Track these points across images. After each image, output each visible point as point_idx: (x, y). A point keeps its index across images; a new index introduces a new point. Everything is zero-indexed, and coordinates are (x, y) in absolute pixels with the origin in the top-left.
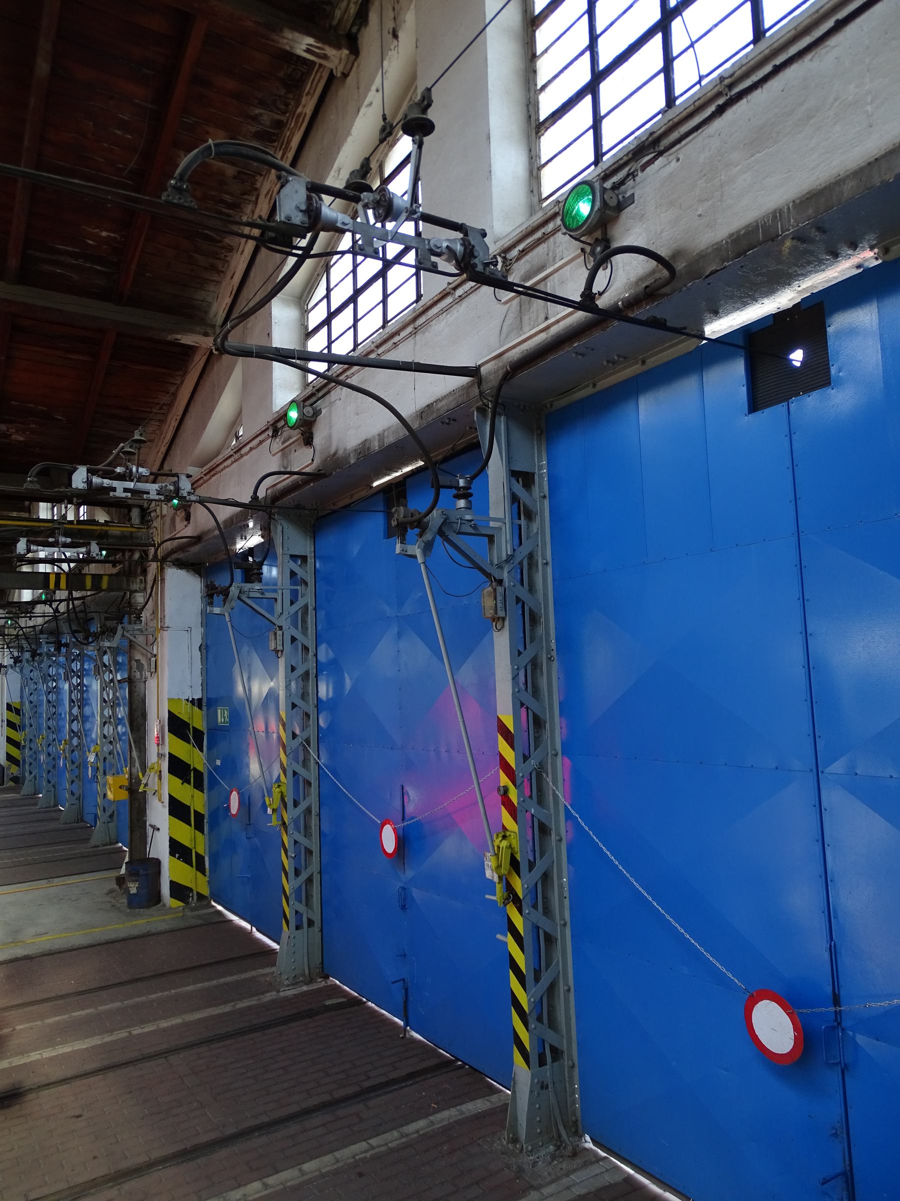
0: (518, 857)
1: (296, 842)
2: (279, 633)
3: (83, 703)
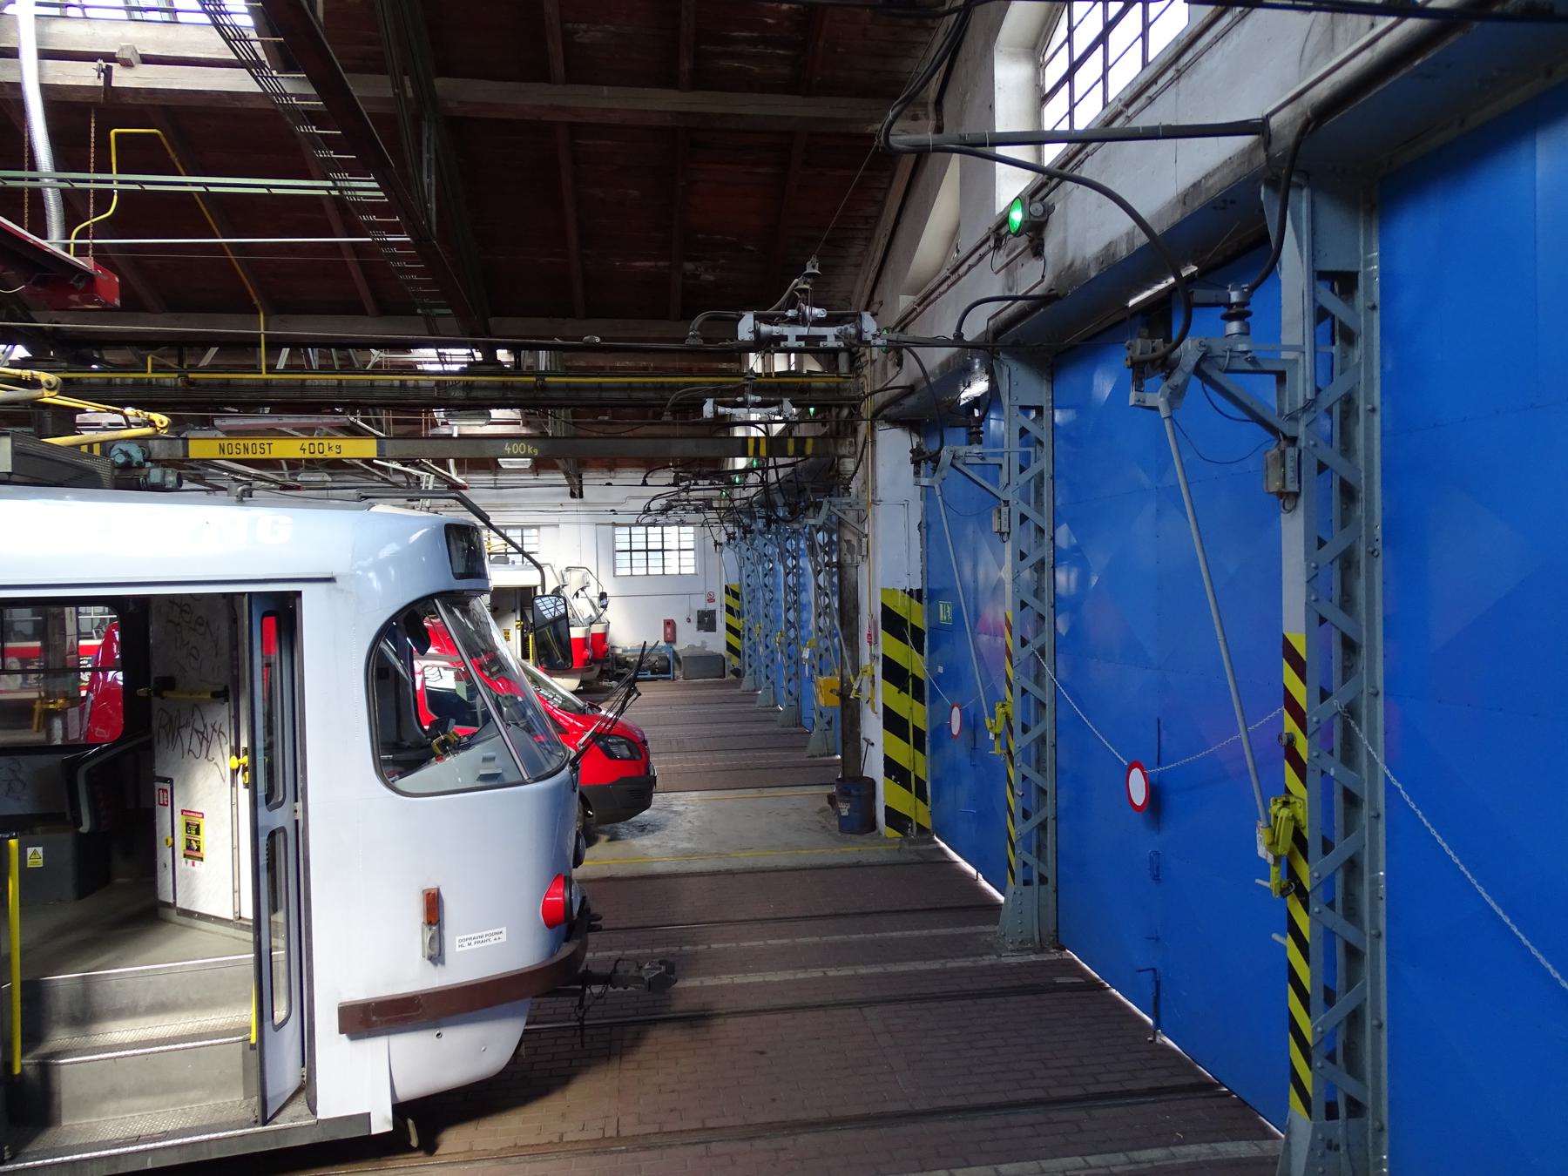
0: (1306, 834)
1: (1024, 778)
2: (1005, 509)
3: (796, 590)
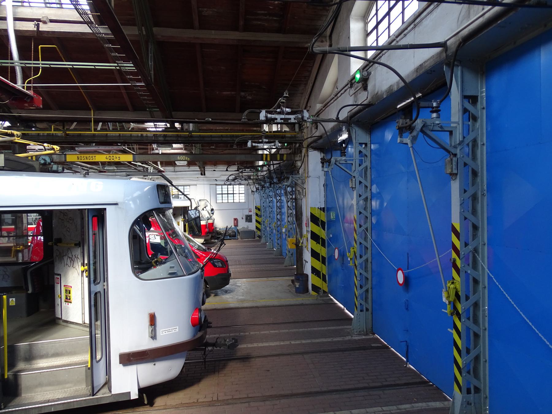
0: (460, 293)
1: (361, 274)
2: (354, 179)
3: (280, 208)
